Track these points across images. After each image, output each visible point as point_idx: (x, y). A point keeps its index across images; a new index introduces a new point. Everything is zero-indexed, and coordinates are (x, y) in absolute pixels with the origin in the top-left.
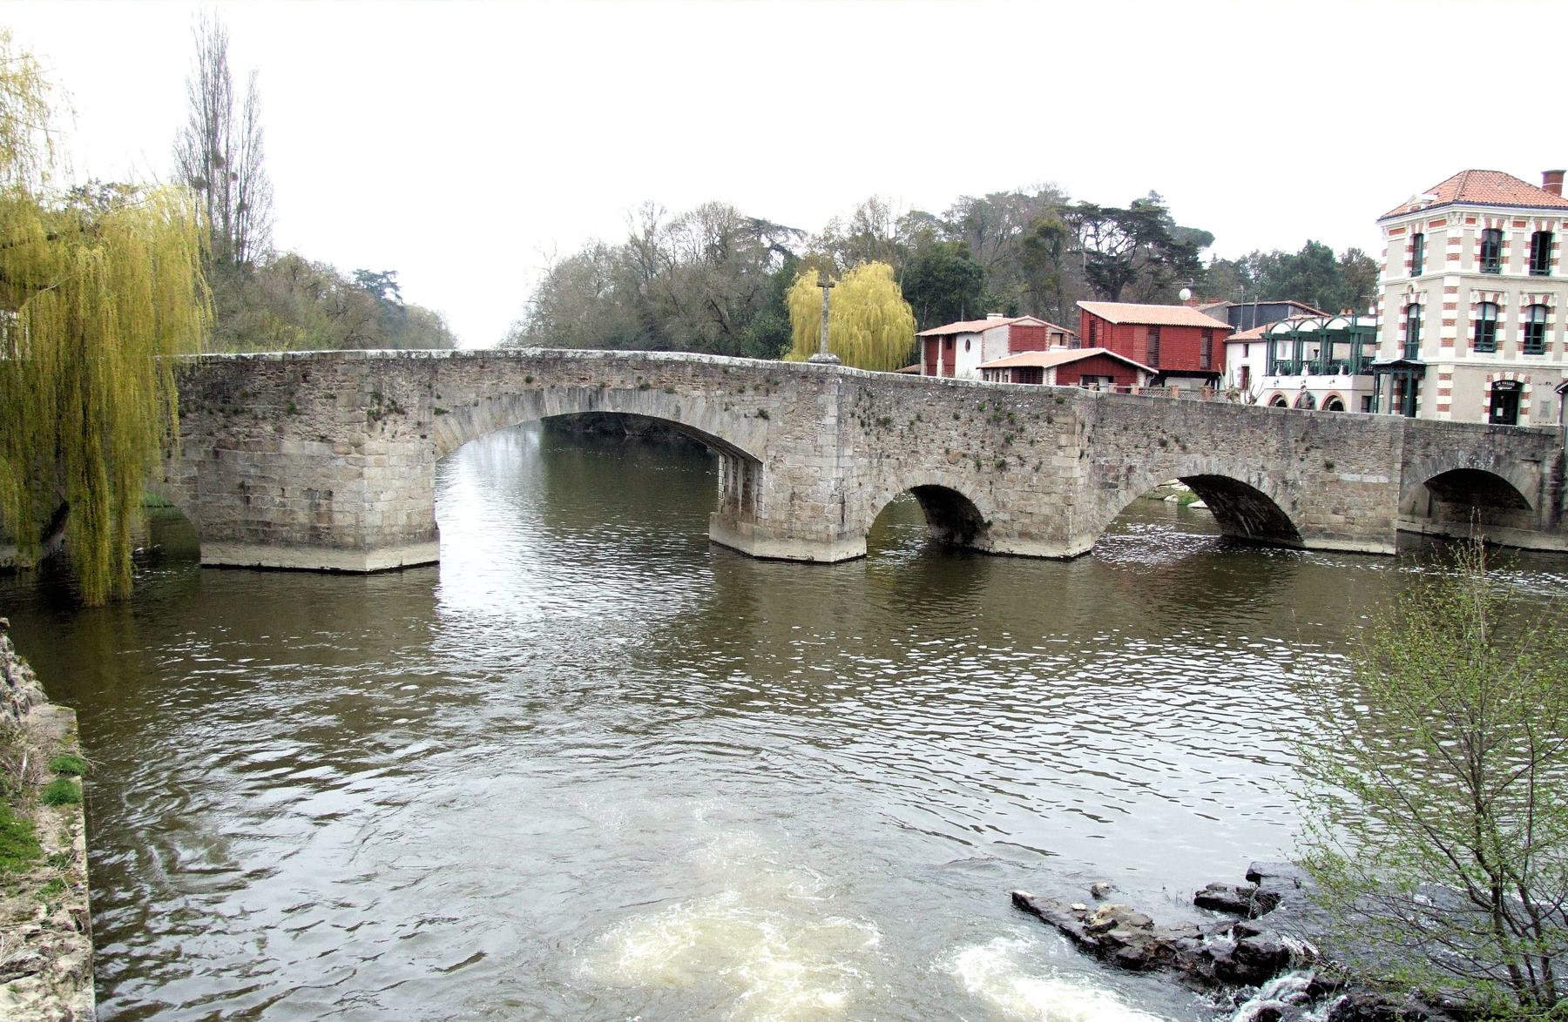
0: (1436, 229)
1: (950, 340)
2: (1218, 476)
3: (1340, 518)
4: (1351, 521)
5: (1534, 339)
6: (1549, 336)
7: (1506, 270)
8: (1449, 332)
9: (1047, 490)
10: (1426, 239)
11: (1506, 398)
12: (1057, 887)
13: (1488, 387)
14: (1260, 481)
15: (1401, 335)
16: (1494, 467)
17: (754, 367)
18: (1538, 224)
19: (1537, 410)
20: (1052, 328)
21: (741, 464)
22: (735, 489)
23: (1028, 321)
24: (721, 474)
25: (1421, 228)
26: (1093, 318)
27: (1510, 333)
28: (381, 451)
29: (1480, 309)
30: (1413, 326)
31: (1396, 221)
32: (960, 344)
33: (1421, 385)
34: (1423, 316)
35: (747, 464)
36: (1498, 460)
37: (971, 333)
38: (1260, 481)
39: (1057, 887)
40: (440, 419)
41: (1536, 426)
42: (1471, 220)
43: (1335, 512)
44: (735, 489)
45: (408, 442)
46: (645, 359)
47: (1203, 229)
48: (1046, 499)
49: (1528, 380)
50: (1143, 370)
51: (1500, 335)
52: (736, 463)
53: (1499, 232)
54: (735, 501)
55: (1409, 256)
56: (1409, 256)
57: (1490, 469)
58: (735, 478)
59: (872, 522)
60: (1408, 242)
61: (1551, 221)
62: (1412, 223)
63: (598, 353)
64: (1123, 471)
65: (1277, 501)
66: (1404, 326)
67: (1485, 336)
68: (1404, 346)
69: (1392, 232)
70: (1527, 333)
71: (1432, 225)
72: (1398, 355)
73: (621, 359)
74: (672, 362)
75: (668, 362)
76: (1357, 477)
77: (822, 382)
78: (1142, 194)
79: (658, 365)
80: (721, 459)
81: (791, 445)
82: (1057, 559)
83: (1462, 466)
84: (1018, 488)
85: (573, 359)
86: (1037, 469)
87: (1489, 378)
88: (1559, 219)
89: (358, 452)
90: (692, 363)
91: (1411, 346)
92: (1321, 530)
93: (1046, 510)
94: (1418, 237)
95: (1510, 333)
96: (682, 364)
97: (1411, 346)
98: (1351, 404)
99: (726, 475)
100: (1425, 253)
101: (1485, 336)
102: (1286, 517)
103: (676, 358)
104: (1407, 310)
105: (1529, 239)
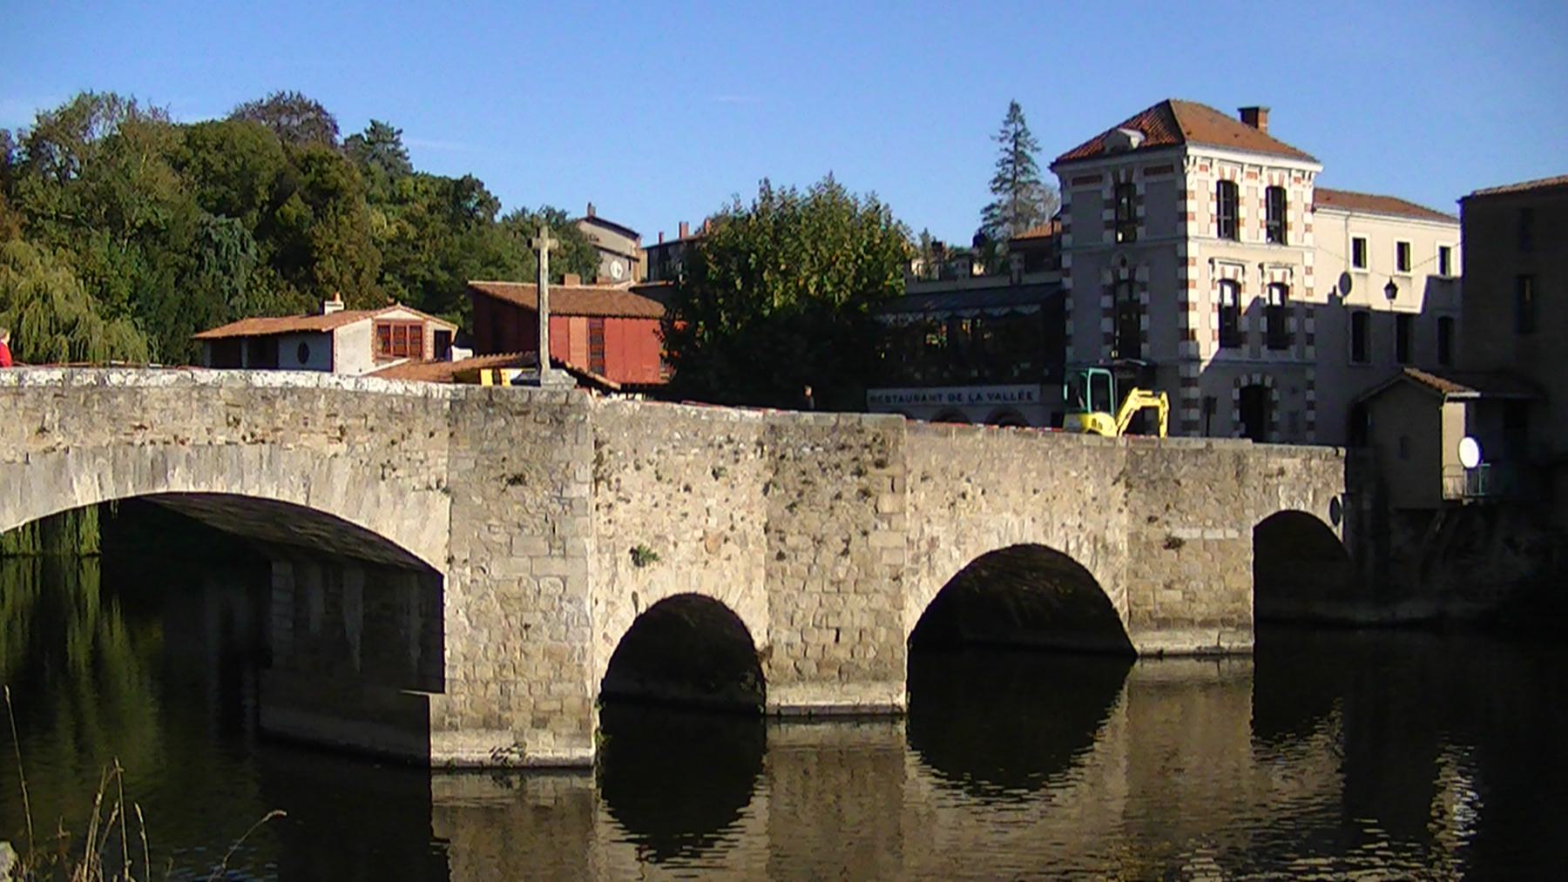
0: (1153, 179)
2: (1034, 544)
3: (1176, 595)
4: (1191, 597)
8: (1381, 260)
12: (785, 440)
13: (1236, 394)
14: (1079, 548)
16: (1313, 507)
20: (433, 325)
38: (1079, 548)
39: (785, 440)
43: (1168, 587)
59: (606, 667)
64: (924, 546)
65: (1098, 577)
69: (1076, 181)
71: (1147, 172)
76: (1196, 533)
77: (560, 422)
79: (268, 397)
83: (1283, 507)
85: (121, 388)
87: (1237, 383)
90: (327, 391)
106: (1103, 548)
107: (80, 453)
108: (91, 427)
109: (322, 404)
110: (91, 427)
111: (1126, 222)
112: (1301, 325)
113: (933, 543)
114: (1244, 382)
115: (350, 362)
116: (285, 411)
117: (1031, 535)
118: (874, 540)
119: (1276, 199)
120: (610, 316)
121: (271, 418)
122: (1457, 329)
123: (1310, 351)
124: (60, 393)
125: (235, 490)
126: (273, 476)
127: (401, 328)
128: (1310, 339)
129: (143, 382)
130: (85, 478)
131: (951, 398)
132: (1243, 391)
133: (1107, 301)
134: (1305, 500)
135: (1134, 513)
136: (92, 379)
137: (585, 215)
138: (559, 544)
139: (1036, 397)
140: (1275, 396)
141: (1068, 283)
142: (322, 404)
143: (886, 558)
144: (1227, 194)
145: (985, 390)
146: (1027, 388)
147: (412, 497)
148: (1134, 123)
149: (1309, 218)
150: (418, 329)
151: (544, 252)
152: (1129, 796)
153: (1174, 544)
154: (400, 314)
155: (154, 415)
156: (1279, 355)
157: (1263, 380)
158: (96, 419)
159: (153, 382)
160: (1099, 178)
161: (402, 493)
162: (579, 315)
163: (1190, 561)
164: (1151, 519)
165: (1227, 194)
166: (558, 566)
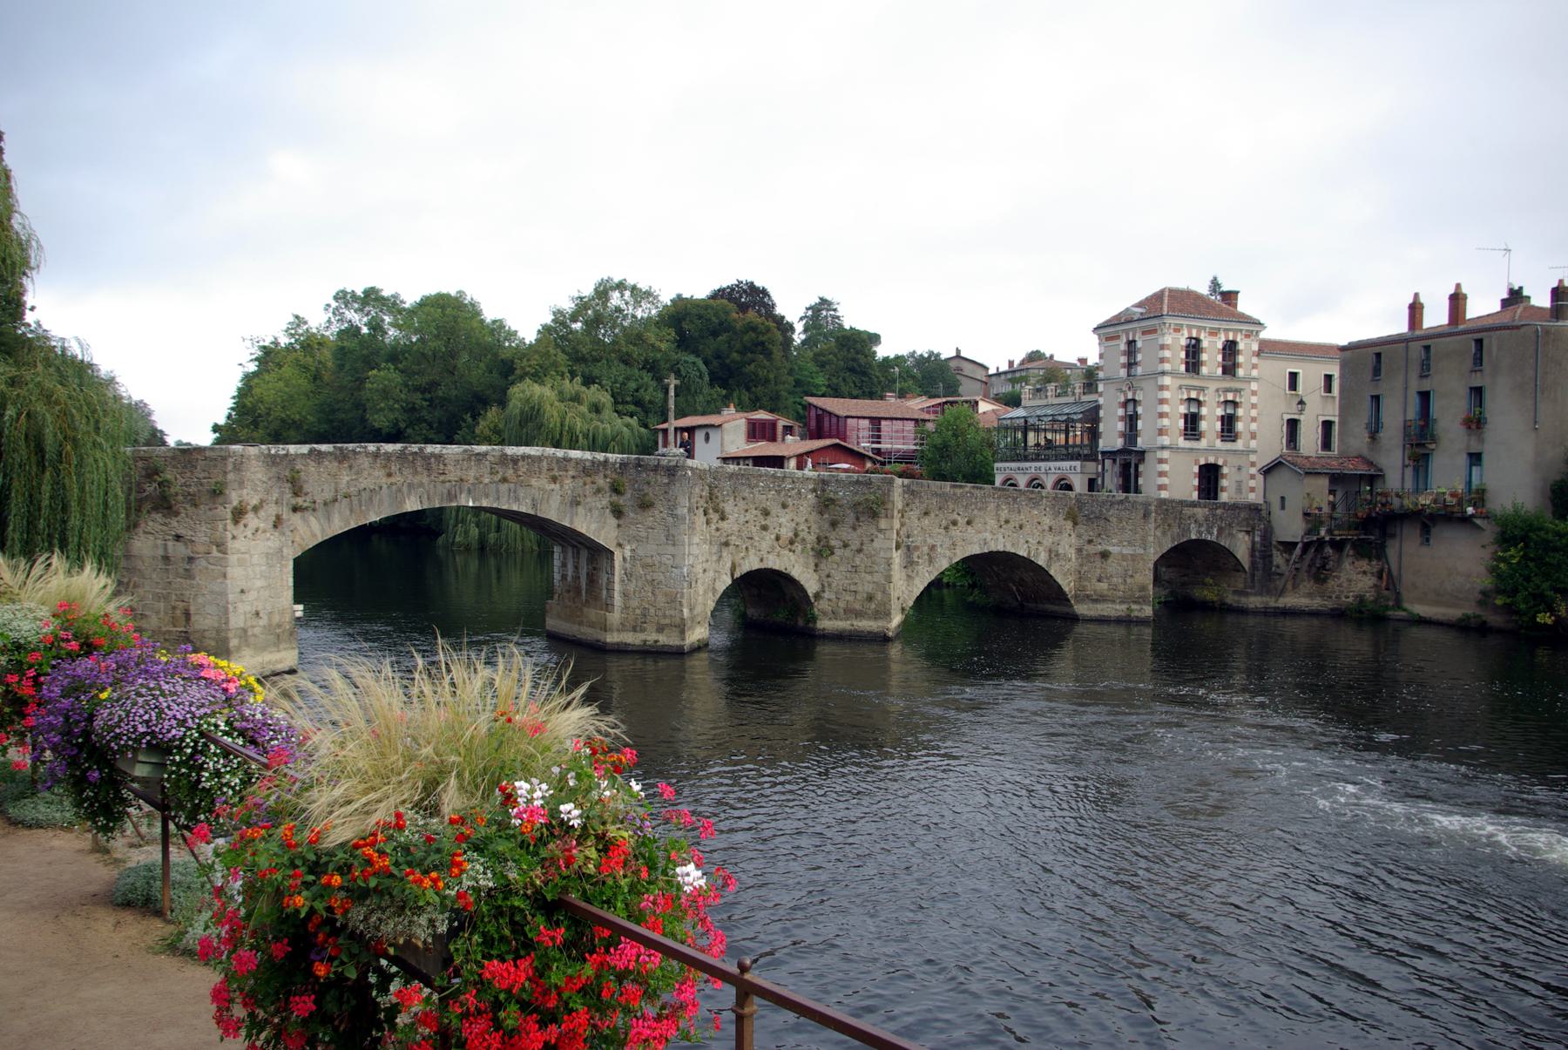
1: (691, 430)
3: (1104, 586)
5: (1228, 426)
6: (1240, 426)
7: (1204, 370)
9: (869, 570)
10: (1139, 344)
11: (1210, 476)
13: (1196, 469)
15: (1121, 426)
17: (606, 461)
18: (1226, 335)
19: (1234, 486)
20: (782, 423)
21: (584, 554)
22: (577, 578)
23: (762, 415)
24: (557, 563)
25: (1134, 335)
26: (820, 412)
27: (1210, 424)
28: (243, 550)
29: (1186, 404)
30: (1132, 420)
31: (1111, 330)
32: (699, 436)
33: (1141, 468)
34: (1140, 410)
35: (597, 553)
36: (1220, 530)
37: (712, 426)
40: (298, 515)
41: (1232, 501)
42: (1178, 331)
44: (577, 578)
45: (268, 539)
46: (504, 456)
47: (872, 331)
48: (869, 577)
49: (1225, 463)
50: (870, 458)
51: (1203, 425)
52: (577, 555)
53: (1198, 340)
54: (578, 590)
55: (1123, 359)
56: (1123, 359)
57: (1214, 539)
58: (576, 568)
59: (713, 605)
60: (1123, 347)
61: (1200, 329)
62: (1126, 332)
63: (305, 449)
65: (1052, 572)
66: (1122, 419)
67: (1192, 424)
68: (1123, 435)
69: (1108, 339)
70: (1186, 423)
71: (1144, 333)
72: (1119, 443)
73: (478, 454)
74: (529, 457)
75: (524, 457)
78: (674, 296)
79: (515, 460)
80: (557, 550)
81: (643, 534)
82: (1119, 621)
83: (1193, 537)
84: (842, 569)
85: (433, 455)
86: (860, 551)
87: (1196, 462)
88: (1241, 331)
89: (219, 551)
91: (1131, 432)
92: (1088, 596)
93: (869, 588)
94: (1131, 343)
95: (1210, 424)
96: (540, 459)
97: (1131, 432)
98: (1079, 484)
99: (564, 565)
100: (1139, 357)
101: (1192, 424)
102: (1060, 586)
103: (533, 453)
104: (1125, 404)
105: (1220, 346)
106: (1053, 554)
107: (410, 486)
108: (416, 473)
109: (545, 463)
110: (416, 473)
111: (1130, 365)
112: (1247, 426)
113: (933, 548)
114: (1202, 462)
115: (732, 442)
116: (523, 467)
117: (1000, 544)
118: (876, 544)
119: (1230, 349)
120: (886, 419)
121: (516, 470)
122: (1336, 429)
123: (1253, 444)
124: (402, 456)
125: (495, 505)
126: (517, 499)
127: (763, 423)
128: (1253, 436)
129: (444, 451)
130: (412, 498)
131: (1036, 468)
132: (1201, 467)
133: (1121, 412)
134: (1211, 534)
135: (1079, 536)
136: (416, 450)
137: (954, 354)
138: (671, 539)
139: (1079, 470)
140: (1225, 470)
141: (1101, 401)
142: (545, 463)
143: (882, 554)
144: (1193, 351)
145: (1052, 464)
146: (1073, 463)
147: (596, 513)
148: (1139, 305)
149: (1255, 360)
150: (774, 424)
151: (672, 386)
152: (100, 563)
153: (1105, 555)
154: (762, 415)
155: (450, 468)
156: (1229, 446)
157: (1217, 459)
158: (419, 469)
159: (450, 451)
160: (1118, 337)
161: (590, 510)
162: (864, 418)
163: (1112, 566)
164: (1090, 542)
165: (1193, 351)
166: (670, 549)
